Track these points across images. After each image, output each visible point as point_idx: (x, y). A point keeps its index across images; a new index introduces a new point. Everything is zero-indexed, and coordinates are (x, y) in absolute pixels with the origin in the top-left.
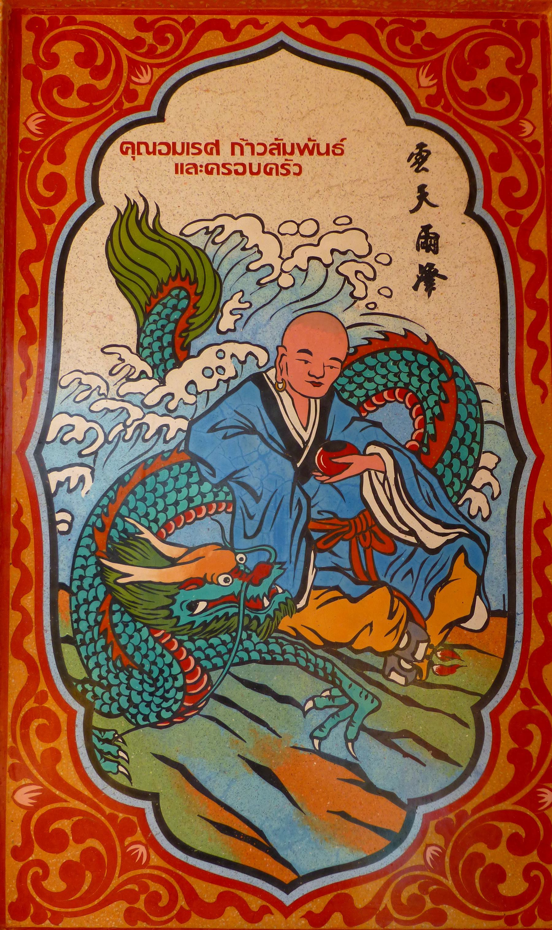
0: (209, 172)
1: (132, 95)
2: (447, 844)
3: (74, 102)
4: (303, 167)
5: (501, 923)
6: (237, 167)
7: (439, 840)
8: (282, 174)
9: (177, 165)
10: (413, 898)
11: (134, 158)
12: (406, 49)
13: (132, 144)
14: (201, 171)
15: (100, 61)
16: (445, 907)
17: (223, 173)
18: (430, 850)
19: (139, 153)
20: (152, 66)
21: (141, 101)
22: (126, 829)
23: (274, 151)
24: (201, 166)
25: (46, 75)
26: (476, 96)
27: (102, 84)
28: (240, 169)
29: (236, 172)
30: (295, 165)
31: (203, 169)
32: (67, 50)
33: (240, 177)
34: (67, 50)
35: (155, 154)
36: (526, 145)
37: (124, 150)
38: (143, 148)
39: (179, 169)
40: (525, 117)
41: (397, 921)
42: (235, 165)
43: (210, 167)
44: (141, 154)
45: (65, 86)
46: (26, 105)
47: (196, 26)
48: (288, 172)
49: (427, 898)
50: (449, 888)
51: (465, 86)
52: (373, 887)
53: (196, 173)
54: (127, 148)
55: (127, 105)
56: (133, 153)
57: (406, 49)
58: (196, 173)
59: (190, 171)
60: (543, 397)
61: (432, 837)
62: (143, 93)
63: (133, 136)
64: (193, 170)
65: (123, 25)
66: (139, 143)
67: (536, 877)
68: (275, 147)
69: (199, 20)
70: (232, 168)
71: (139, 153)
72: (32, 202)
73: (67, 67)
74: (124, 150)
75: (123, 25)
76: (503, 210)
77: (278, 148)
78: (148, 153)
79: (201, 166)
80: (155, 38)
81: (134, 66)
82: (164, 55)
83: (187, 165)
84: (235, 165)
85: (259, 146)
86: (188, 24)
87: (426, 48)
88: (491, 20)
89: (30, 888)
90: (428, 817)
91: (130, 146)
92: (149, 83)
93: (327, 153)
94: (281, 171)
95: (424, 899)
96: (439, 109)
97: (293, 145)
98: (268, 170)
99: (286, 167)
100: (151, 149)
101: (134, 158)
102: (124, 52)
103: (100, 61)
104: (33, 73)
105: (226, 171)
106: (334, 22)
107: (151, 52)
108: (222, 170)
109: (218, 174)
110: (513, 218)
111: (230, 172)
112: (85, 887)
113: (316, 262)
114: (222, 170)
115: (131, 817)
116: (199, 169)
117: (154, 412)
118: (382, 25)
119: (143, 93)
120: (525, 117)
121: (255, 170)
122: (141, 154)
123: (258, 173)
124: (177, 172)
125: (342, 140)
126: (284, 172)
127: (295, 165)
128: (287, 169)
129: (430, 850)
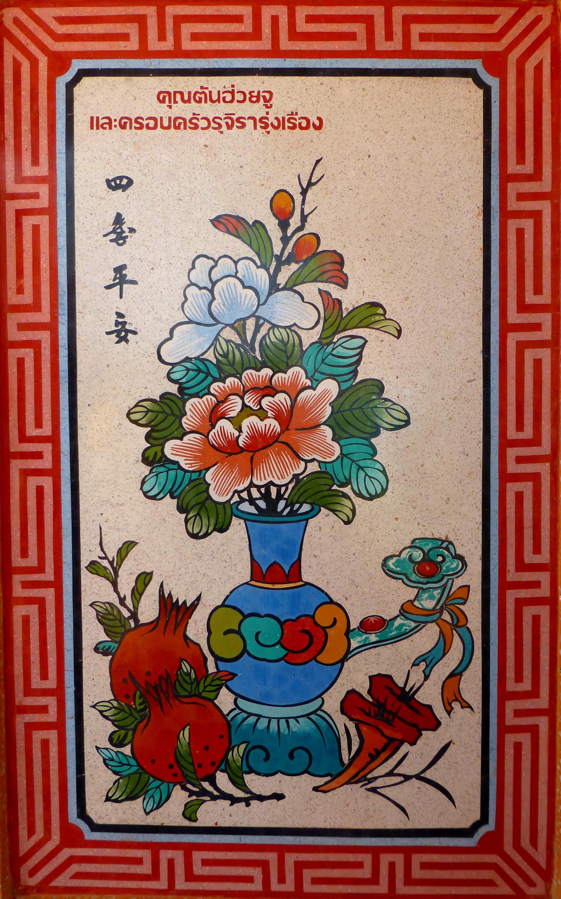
0: (123, 127)
6: (301, 121)
8: (190, 128)
9: (92, 118)
13: (169, 93)
19: (176, 102)
24: (115, 120)
28: (152, 123)
29: (148, 127)
31: (117, 123)
37: (161, 99)
42: (147, 119)
48: (196, 127)
53: (110, 128)
56: (170, 102)
59: (105, 126)
60: (258, 634)
64: (107, 126)
66: (175, 93)
68: (107, 121)
70: (145, 123)
71: (176, 102)
74: (161, 99)
83: (102, 119)
84: (147, 119)
85: (239, 94)
93: (218, 100)
99: (241, 120)
100: (186, 98)
101: (170, 107)
108: (134, 125)
109: (131, 128)
111: (141, 128)
114: (134, 125)
116: (114, 123)
117: (317, 323)
121: (166, 124)
124: (92, 128)
127: (202, 118)
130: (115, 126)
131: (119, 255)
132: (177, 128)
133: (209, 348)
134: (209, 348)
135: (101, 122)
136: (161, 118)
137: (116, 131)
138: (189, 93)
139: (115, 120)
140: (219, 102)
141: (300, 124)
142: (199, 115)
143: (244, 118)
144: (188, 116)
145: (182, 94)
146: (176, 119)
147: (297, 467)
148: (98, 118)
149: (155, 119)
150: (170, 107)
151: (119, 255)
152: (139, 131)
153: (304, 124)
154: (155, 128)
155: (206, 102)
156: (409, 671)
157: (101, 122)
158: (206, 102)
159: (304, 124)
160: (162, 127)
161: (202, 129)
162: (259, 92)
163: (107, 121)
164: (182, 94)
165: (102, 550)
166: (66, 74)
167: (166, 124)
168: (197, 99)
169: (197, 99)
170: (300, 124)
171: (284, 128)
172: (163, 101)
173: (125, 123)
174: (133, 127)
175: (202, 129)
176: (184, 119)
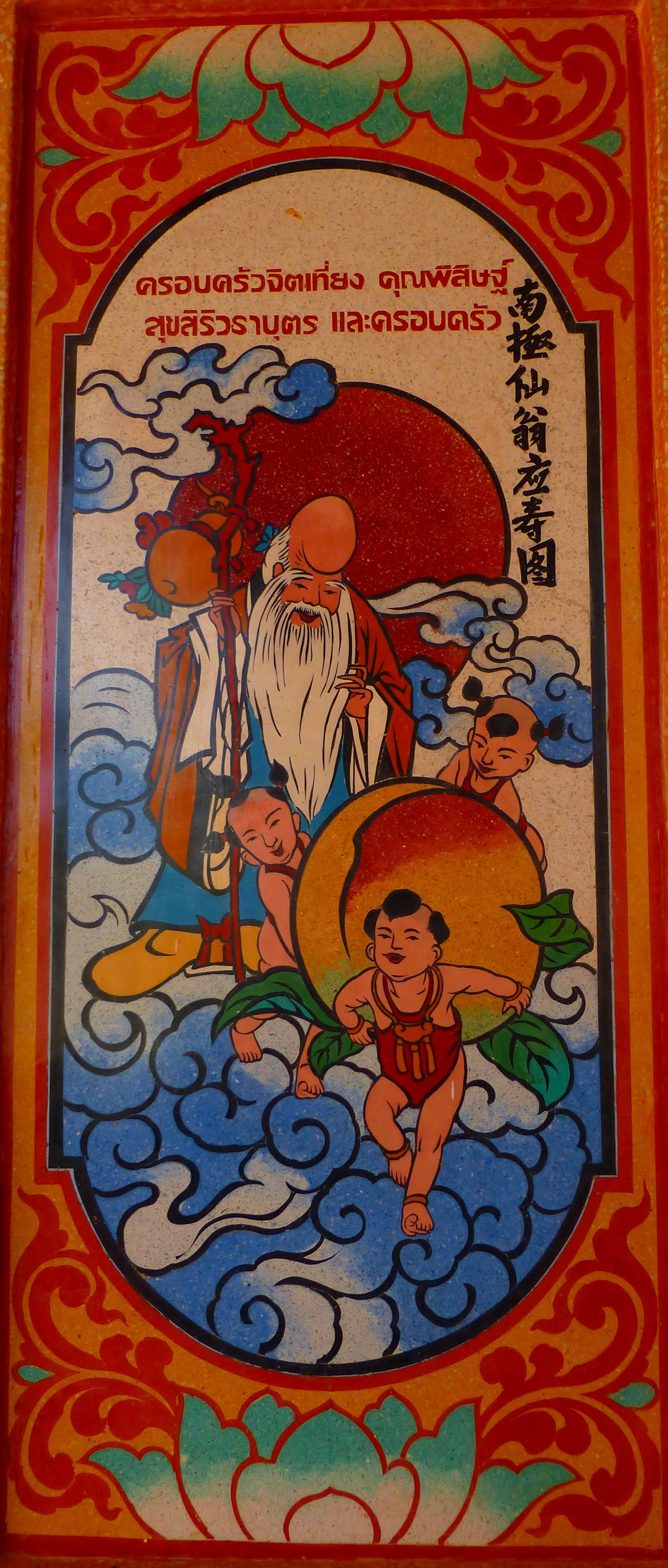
0: (378, 327)
6: (414, 317)
9: (334, 314)
11: (397, 294)
14: (367, 326)
17: (473, 328)
19: (404, 287)
23: (460, 281)
30: (489, 312)
33: (437, 333)
38: (408, 278)
53: (360, 330)
54: (147, 286)
56: (397, 286)
58: (360, 330)
66: (404, 273)
68: (355, 318)
71: (404, 287)
77: (466, 278)
78: (416, 285)
79: (367, 317)
84: (413, 313)
91: (151, 283)
97: (423, 273)
101: (397, 294)
105: (400, 324)
108: (395, 323)
111: (404, 327)
113: (143, 474)
116: (365, 322)
125: (505, 262)
127: (218, 318)
128: (209, 326)
130: (367, 326)
132: (455, 327)
133: (258, 860)
134: (258, 860)
137: (369, 333)
139: (367, 317)
141: (413, 321)
142: (486, 307)
143: (244, 318)
146: (217, 278)
148: (342, 314)
152: (399, 333)
155: (301, 290)
157: (182, 324)
158: (301, 290)
159: (184, 286)
160: (198, 289)
161: (254, 290)
162: (345, 275)
163: (355, 318)
166: (576, 237)
167: (202, 285)
168: (290, 285)
169: (290, 285)
170: (413, 321)
171: (298, 332)
172: (387, 286)
173: (381, 321)
174: (393, 328)
175: (254, 290)
176: (464, 314)
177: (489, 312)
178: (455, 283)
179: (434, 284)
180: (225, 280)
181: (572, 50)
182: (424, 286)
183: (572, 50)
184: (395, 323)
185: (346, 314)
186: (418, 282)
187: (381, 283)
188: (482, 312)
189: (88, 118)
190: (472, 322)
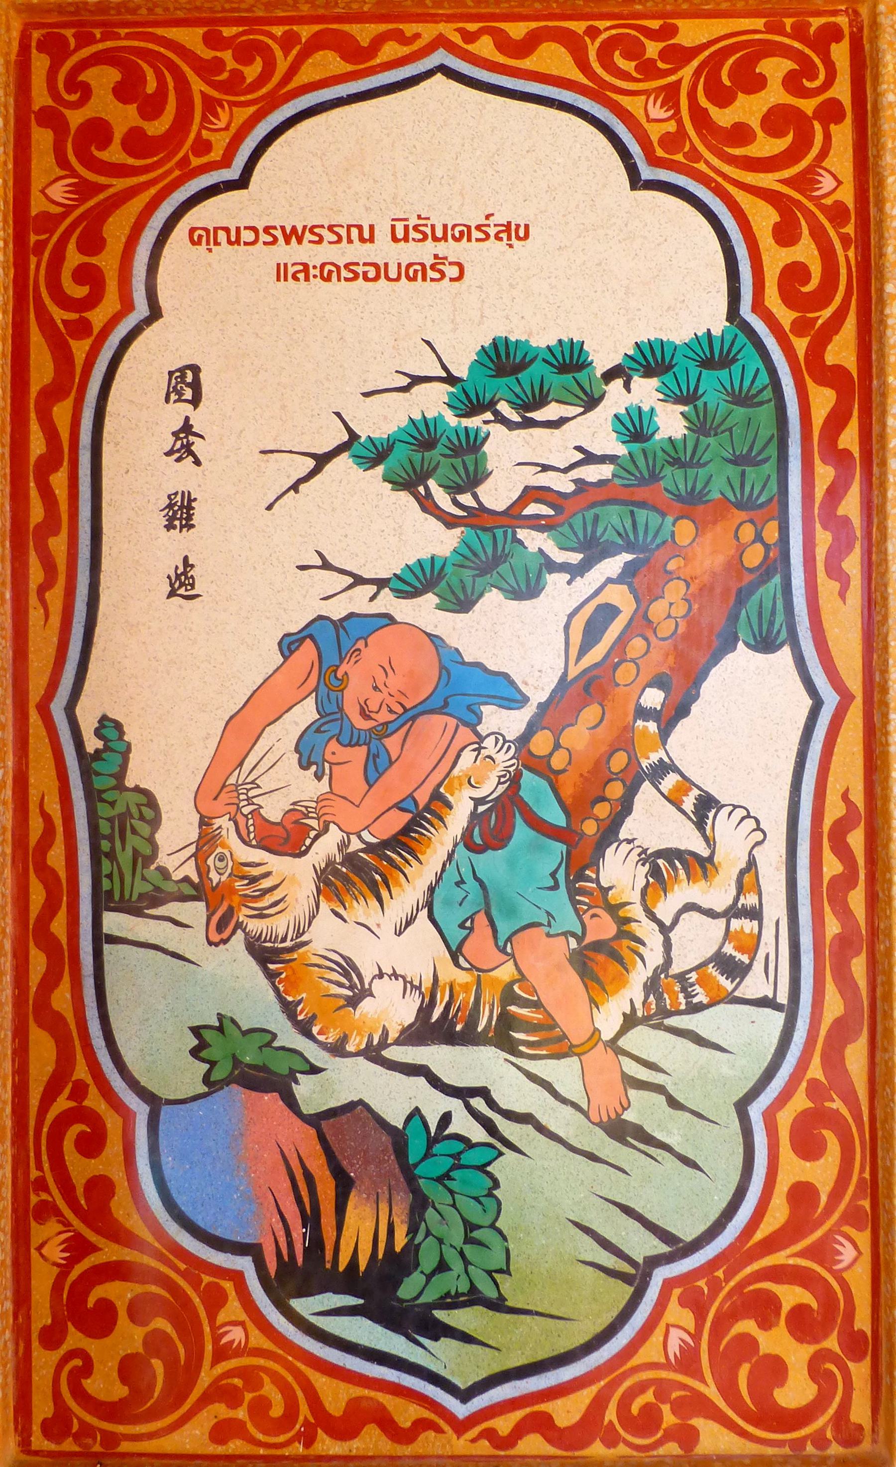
1: (202, 147)
2: (699, 1326)
3: (791, 1296)
4: (466, 265)
5: (787, 1450)
6: (367, 268)
7: (687, 1318)
9: (278, 265)
10: (647, 1409)
12: (628, 66)
14: (315, 276)
15: (151, 86)
16: (698, 1422)
18: (676, 1336)
19: (217, 243)
20: (232, 104)
21: (216, 155)
22: (672, 141)
25: (75, 118)
26: (741, 134)
27: (157, 127)
29: (366, 278)
30: (450, 264)
31: (317, 272)
32: (102, 79)
33: (370, 283)
34: (102, 79)
35: (239, 244)
36: (823, 208)
37: (196, 238)
38: (222, 235)
39: (282, 272)
40: (823, 164)
41: (272, 36)
42: (365, 264)
43: (328, 268)
44: (219, 244)
45: (802, 1324)
46: (42, 163)
47: (303, 40)
49: (666, 1409)
50: (199, 75)
51: (723, 117)
52: (584, 1398)
53: (307, 279)
55: (196, 162)
56: (208, 243)
57: (628, 66)
58: (307, 279)
61: (678, 1314)
62: (220, 142)
63: (205, 214)
64: (301, 276)
65: (713, 1438)
66: (216, 229)
67: (69, 91)
68: (301, 268)
69: (305, 32)
70: (360, 269)
71: (217, 243)
72: (845, 1111)
73: (104, 104)
75: (713, 1438)
76: (786, 317)
80: (236, 59)
81: (688, 1361)
82: (641, 1387)
83: (293, 265)
84: (365, 264)
85: (248, 231)
86: (288, 42)
87: (661, 65)
88: (764, 20)
89: (817, 60)
90: (668, 1285)
92: (227, 128)
94: (431, 274)
95: (660, 1411)
96: (679, 157)
98: (411, 274)
101: (210, 250)
102: (711, 1391)
103: (151, 86)
104: (51, 118)
106: (517, 30)
107: (662, 1389)
108: (344, 273)
109: (339, 280)
110: (800, 327)
112: (731, 61)
115: (667, 156)
116: (312, 272)
118: (593, 32)
119: (220, 142)
120: (823, 164)
121: (393, 274)
122: (219, 244)
123: (398, 279)
124: (278, 279)
126: (437, 275)
129: (221, 125)
131: (180, 477)
135: (291, 270)
136: (386, 265)
138: (445, 227)
140: (446, 241)
142: (446, 258)
144: (429, 261)
145: (360, 228)
146: (409, 265)
147: (432, 830)
148: (286, 265)
149: (376, 265)
150: (210, 250)
151: (180, 477)
153: (372, 274)
154: (377, 278)
156: (505, 1239)
159: (372, 274)
160: (388, 278)
161: (451, 280)
163: (301, 268)
164: (227, 230)
165: (283, 1048)
167: (393, 274)
172: (199, 243)
174: (473, 239)
175: (451, 280)
176: (423, 265)
177: (450, 264)
178: (295, 278)
179: (288, 241)
180: (418, 267)
181: (61, 85)
182: (446, 241)
183: (61, 85)
184: (344, 273)
185: (289, 266)
186: (233, 239)
187: (193, 243)
188: (444, 264)
189: (79, 1183)
190: (431, 274)
